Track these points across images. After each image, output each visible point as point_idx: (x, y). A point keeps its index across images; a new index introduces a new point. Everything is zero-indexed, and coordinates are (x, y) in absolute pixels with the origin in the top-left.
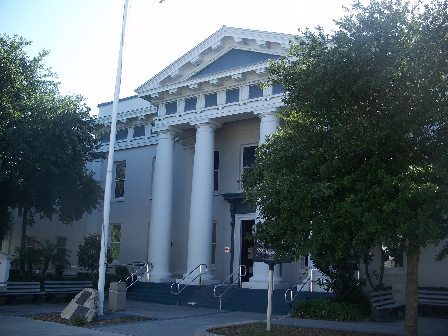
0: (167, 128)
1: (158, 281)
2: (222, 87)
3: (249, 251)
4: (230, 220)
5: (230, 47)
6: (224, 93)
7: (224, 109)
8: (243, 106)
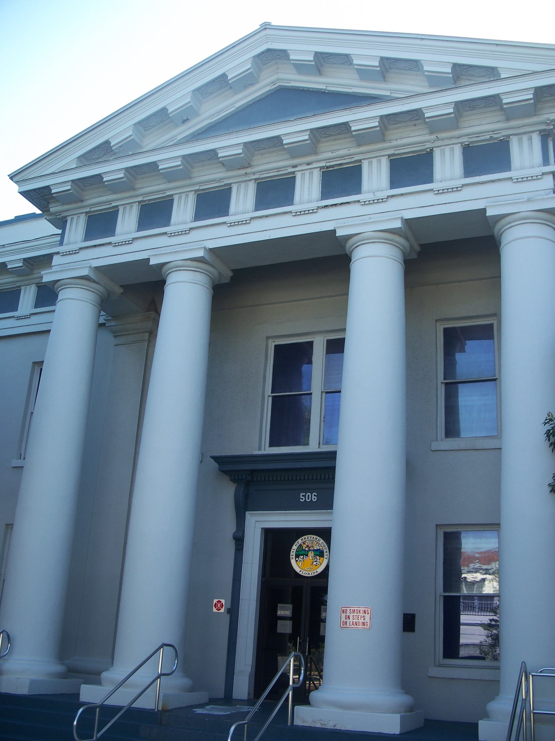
0: (85, 272)
1: (24, 690)
2: (249, 170)
3: (280, 613)
4: (231, 527)
5: (273, 83)
6: (252, 188)
7: (249, 225)
8: (306, 216)
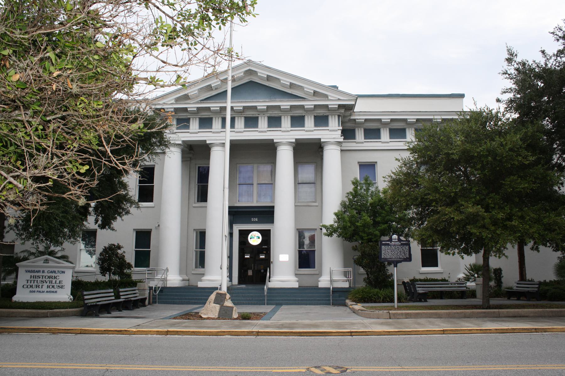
8: (262, 132)
